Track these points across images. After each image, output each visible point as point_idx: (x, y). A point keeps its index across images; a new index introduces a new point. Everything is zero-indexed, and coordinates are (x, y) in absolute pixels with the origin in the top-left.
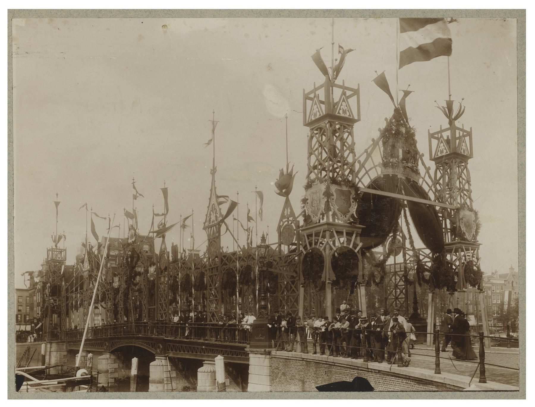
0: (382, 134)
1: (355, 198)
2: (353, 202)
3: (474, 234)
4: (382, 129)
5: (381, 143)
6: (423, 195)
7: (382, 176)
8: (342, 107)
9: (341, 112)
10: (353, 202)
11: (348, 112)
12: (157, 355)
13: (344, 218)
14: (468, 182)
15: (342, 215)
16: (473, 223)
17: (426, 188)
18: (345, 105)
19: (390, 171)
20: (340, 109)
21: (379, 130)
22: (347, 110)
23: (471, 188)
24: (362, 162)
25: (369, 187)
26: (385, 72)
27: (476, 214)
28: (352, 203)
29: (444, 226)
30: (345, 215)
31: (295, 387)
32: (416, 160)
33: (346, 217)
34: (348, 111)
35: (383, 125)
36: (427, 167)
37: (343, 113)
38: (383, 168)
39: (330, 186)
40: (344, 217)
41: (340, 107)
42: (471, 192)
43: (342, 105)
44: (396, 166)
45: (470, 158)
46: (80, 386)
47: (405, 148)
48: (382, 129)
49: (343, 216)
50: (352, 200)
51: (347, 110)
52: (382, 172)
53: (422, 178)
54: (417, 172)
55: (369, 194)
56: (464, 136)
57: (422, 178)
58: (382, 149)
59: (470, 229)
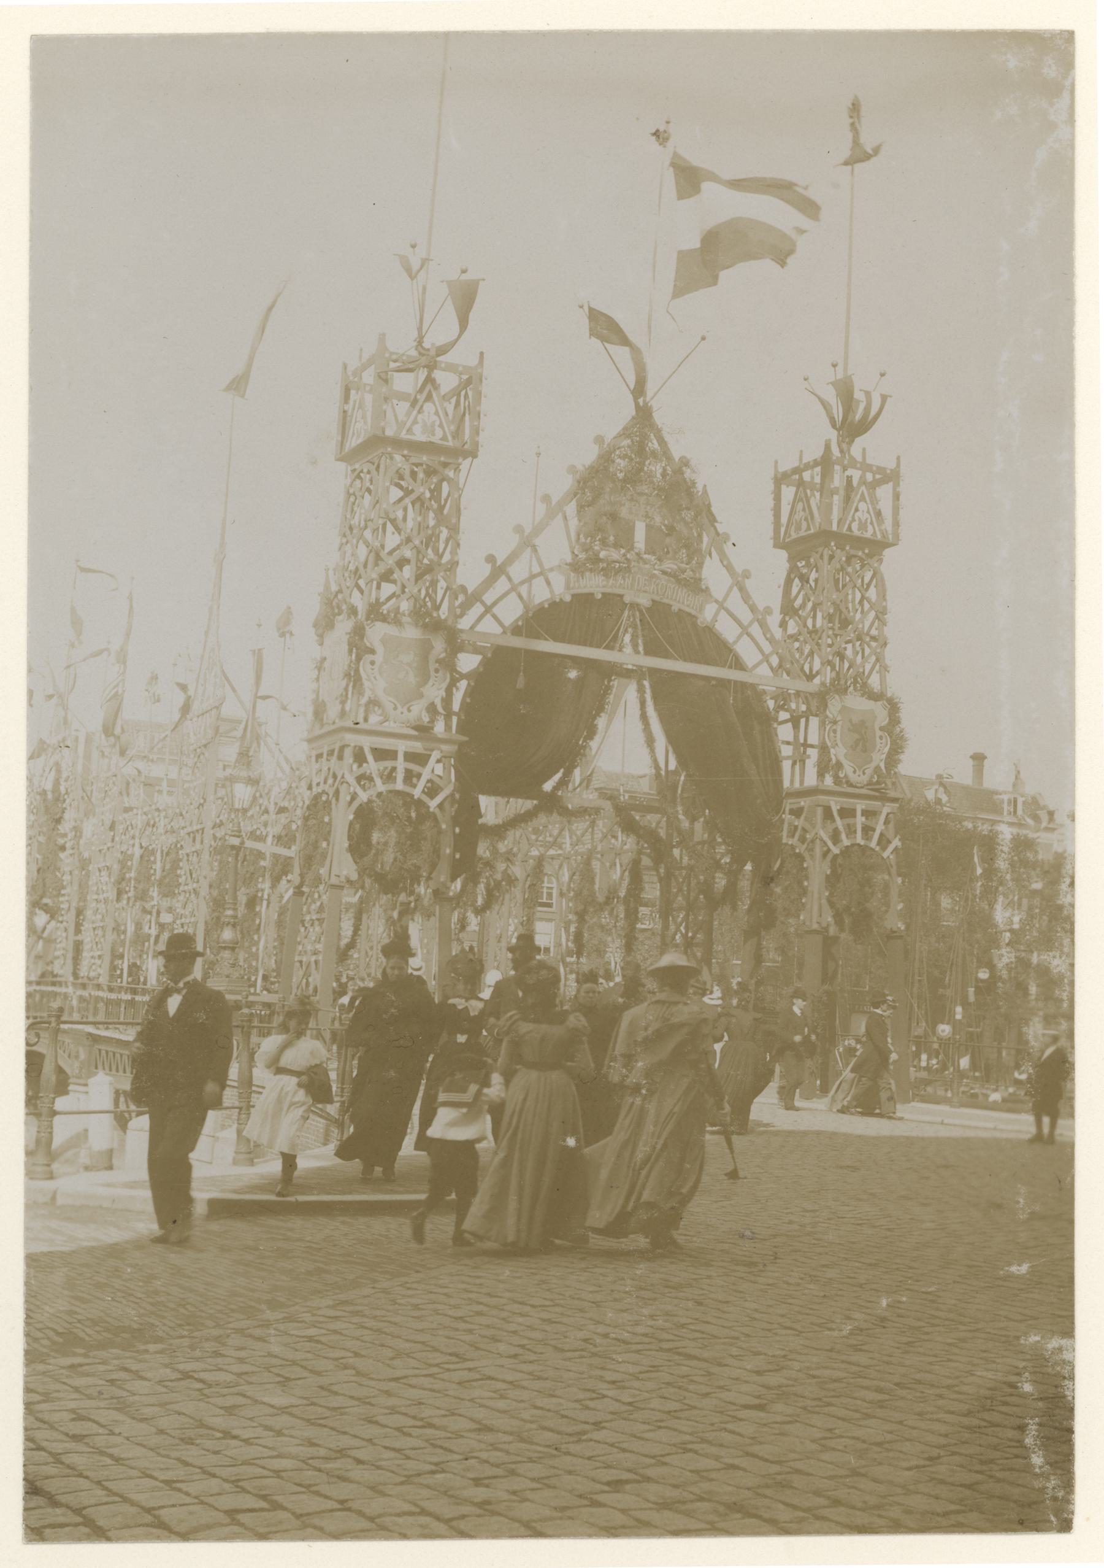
0: (579, 482)
1: (443, 659)
2: (437, 671)
3: (878, 768)
4: (580, 468)
5: (571, 508)
6: (724, 653)
7: (568, 598)
8: (858, 514)
9: (855, 526)
10: (437, 671)
11: (870, 528)
12: (75, 1080)
13: (402, 713)
14: (881, 615)
15: (399, 706)
16: (879, 733)
17: (727, 630)
18: (866, 510)
19: (595, 584)
20: (853, 520)
21: (572, 469)
22: (869, 521)
23: (888, 631)
24: (499, 563)
25: (516, 631)
26: (481, 283)
27: (893, 707)
28: (432, 673)
29: (455, 719)
30: (407, 706)
31: (1069, 1085)
32: (694, 553)
33: (409, 710)
34: (872, 523)
35: (589, 456)
36: (739, 569)
37: (859, 530)
38: (572, 574)
39: (367, 628)
40: (405, 710)
41: (854, 515)
42: (885, 644)
43: (857, 510)
44: (620, 570)
45: (889, 545)
46: (334, 1093)
47: (658, 520)
48: (580, 468)
49: (400, 709)
50: (433, 666)
51: (869, 521)
52: (567, 587)
53: (716, 601)
54: (696, 586)
55: (515, 651)
56: (874, 485)
57: (716, 601)
58: (574, 523)
59: (865, 751)
